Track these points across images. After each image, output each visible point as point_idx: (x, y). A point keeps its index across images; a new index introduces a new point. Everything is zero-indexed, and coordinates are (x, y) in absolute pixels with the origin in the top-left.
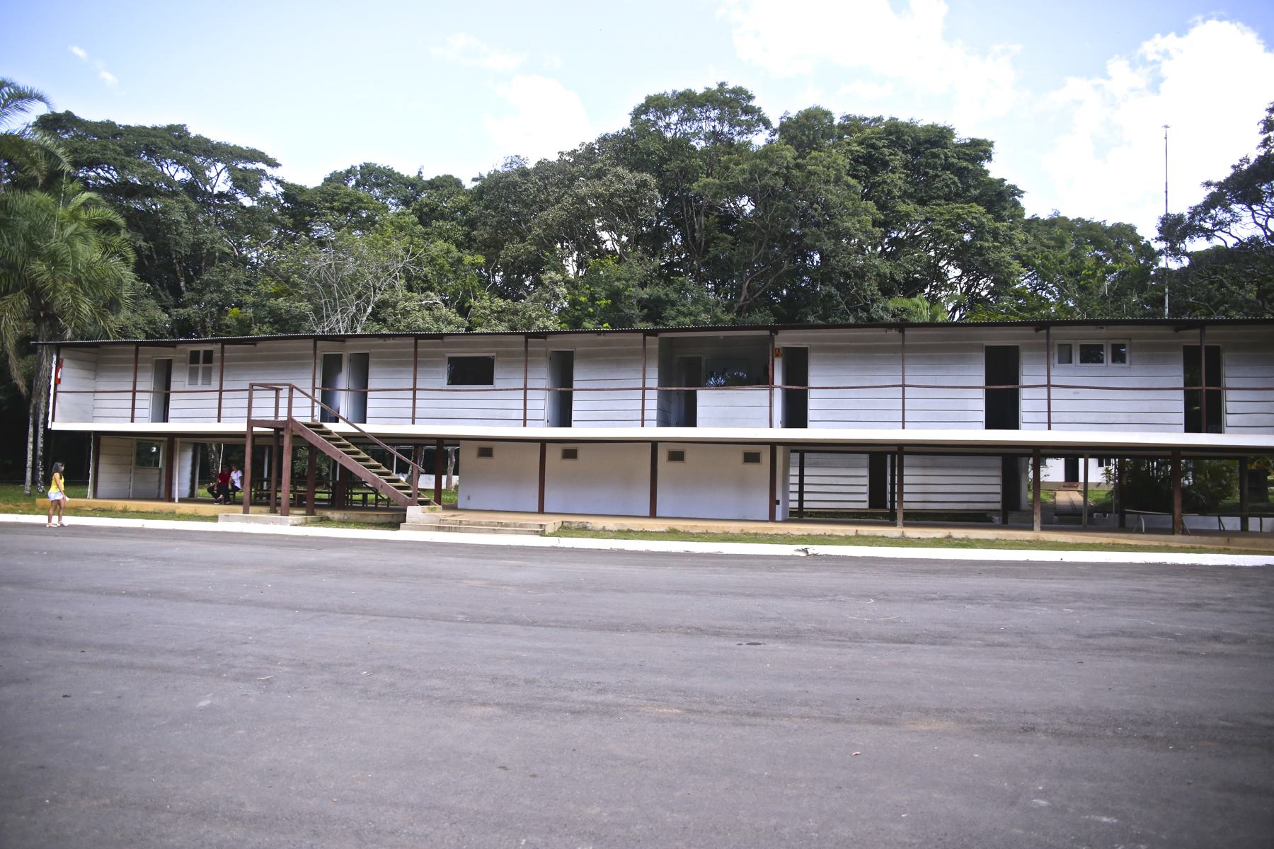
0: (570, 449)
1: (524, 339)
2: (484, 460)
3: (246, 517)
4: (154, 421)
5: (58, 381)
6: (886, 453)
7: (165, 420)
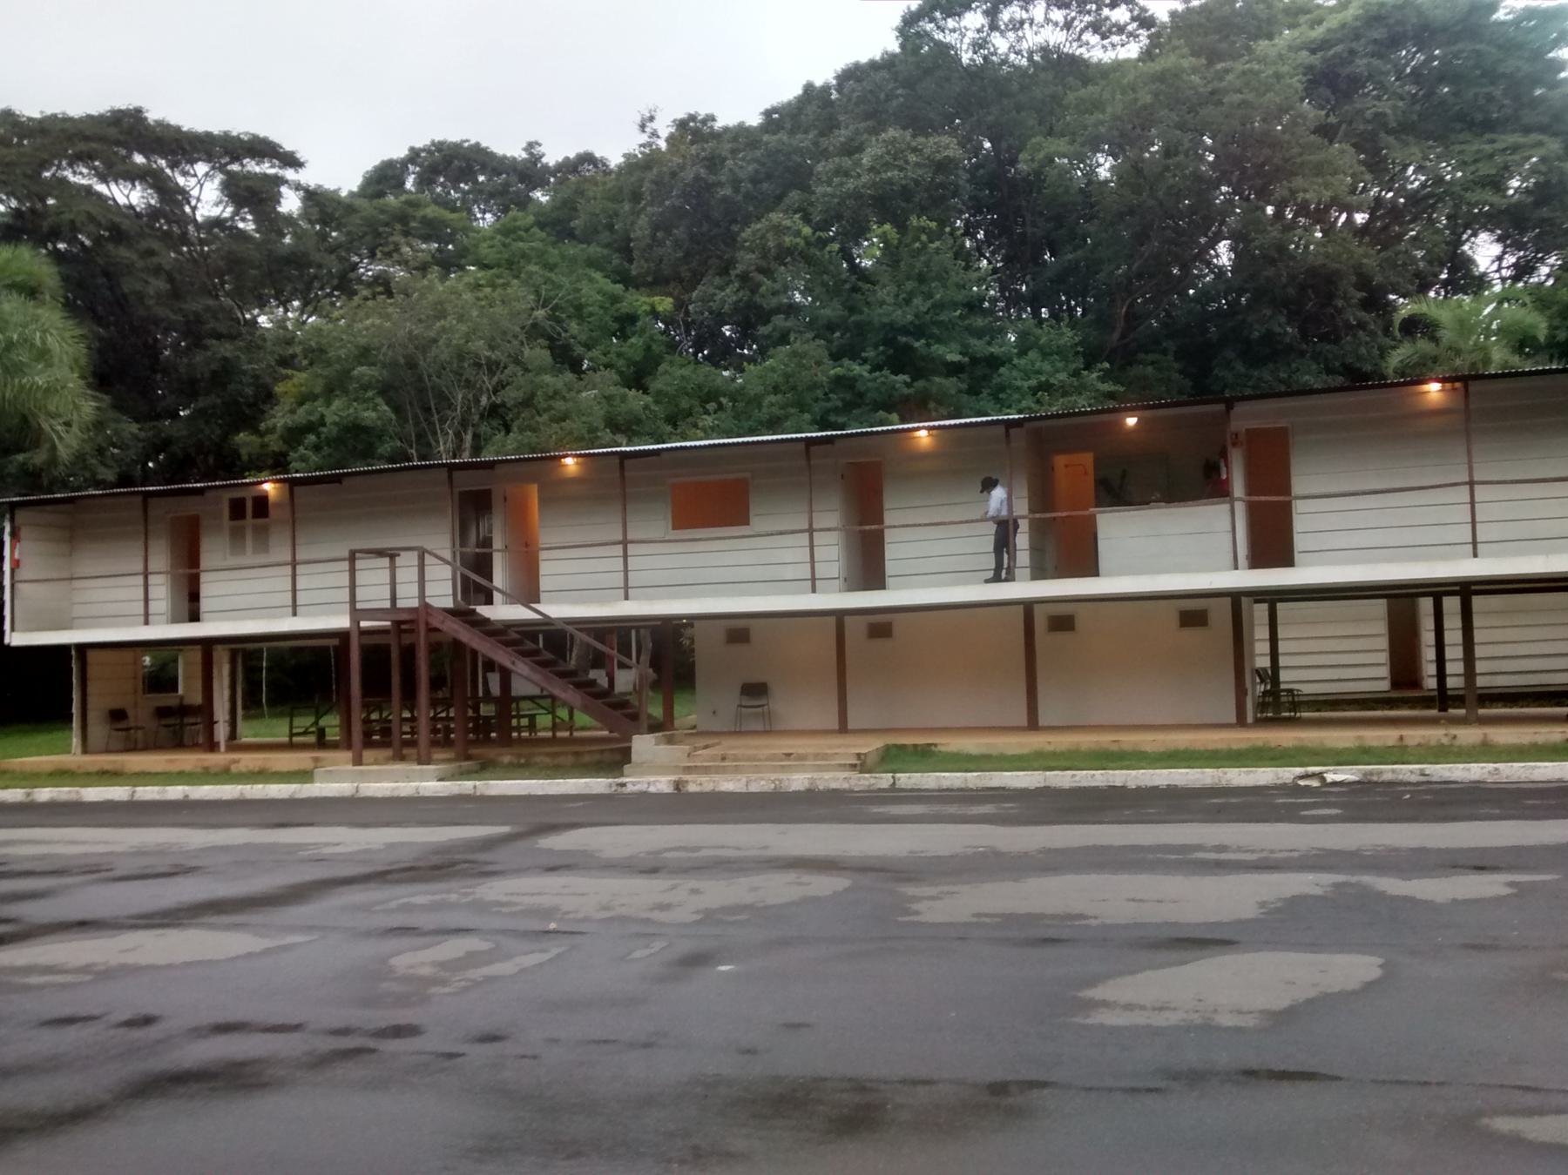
0: (881, 625)
1: (618, 461)
2: (879, 643)
3: (361, 771)
4: (175, 620)
5: (16, 565)
6: (632, 627)
7: (194, 617)
